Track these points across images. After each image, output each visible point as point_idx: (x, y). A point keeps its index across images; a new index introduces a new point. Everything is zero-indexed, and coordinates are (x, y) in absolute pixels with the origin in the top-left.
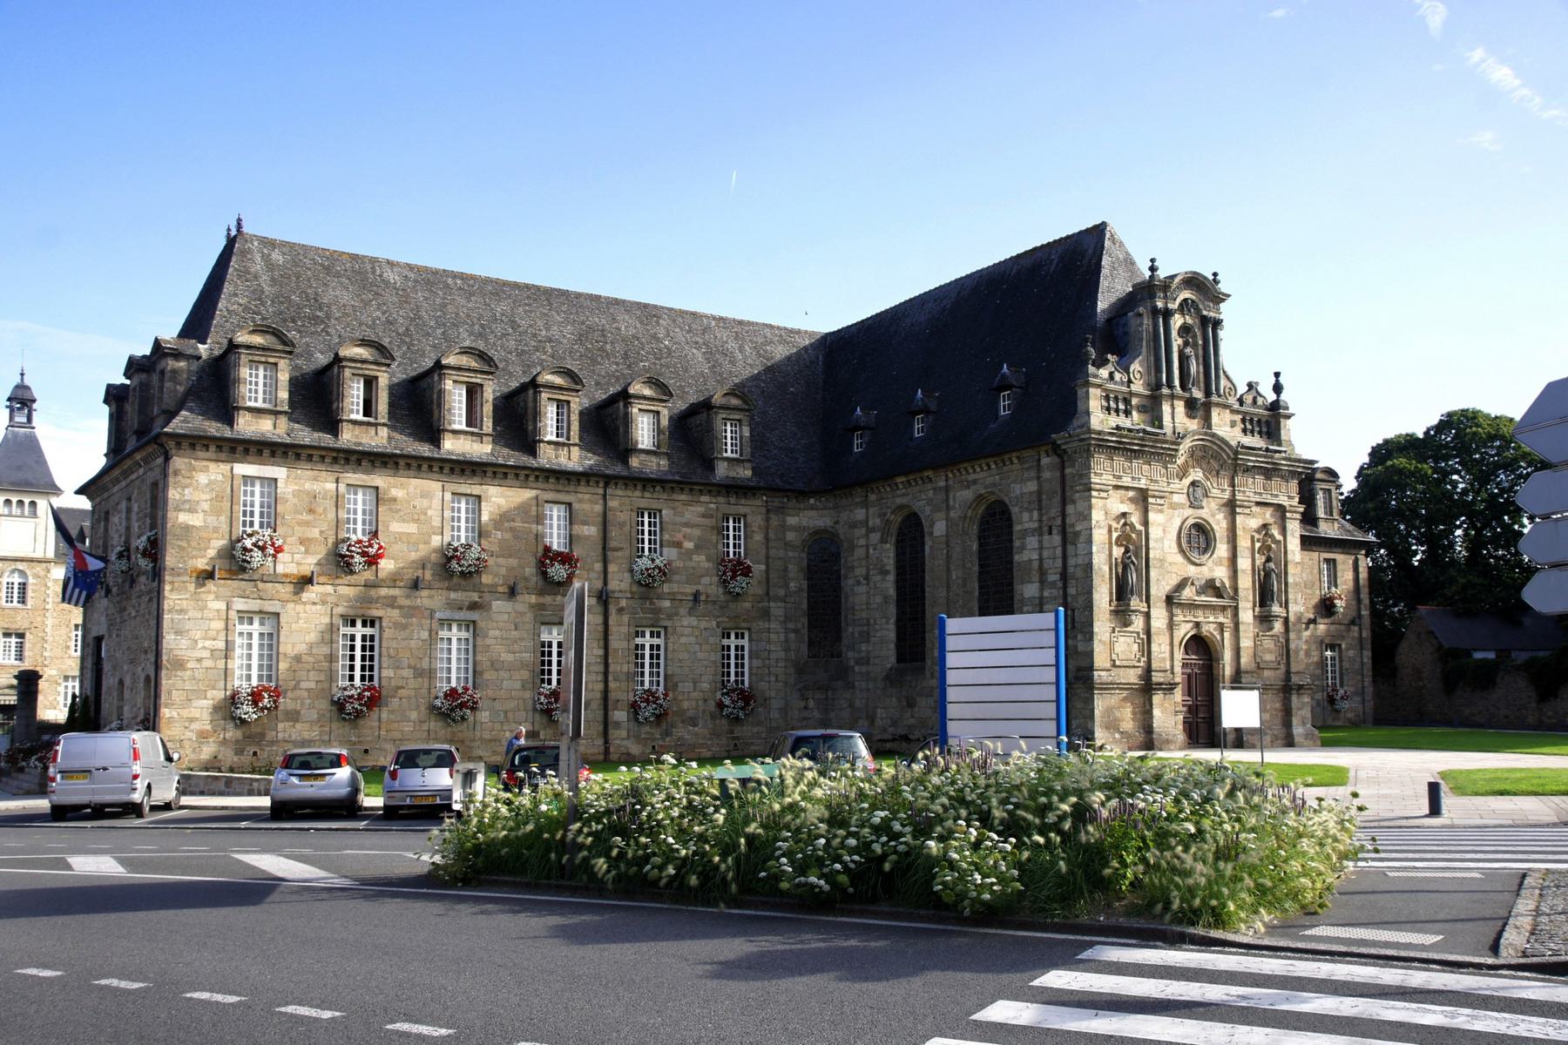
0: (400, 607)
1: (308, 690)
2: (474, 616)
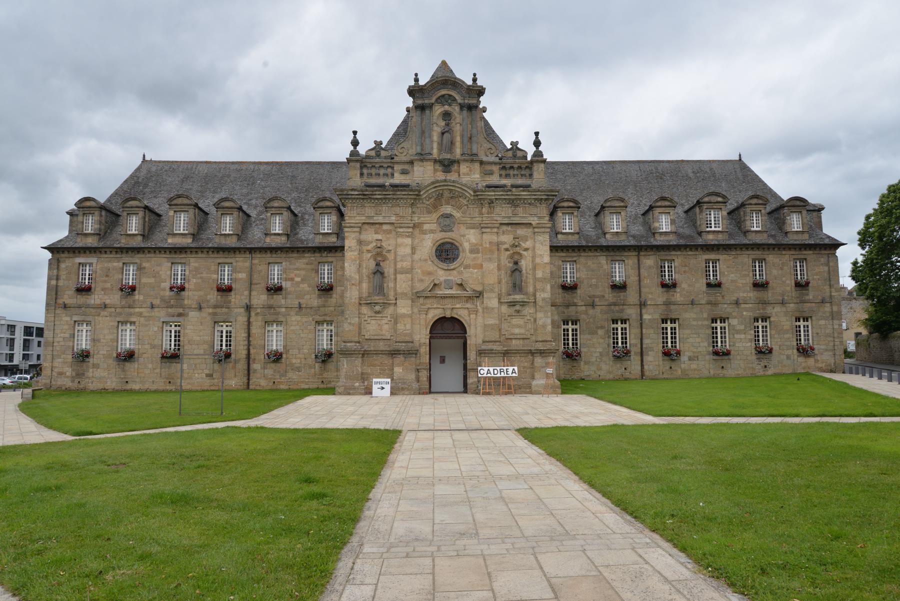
2: (180, 319)
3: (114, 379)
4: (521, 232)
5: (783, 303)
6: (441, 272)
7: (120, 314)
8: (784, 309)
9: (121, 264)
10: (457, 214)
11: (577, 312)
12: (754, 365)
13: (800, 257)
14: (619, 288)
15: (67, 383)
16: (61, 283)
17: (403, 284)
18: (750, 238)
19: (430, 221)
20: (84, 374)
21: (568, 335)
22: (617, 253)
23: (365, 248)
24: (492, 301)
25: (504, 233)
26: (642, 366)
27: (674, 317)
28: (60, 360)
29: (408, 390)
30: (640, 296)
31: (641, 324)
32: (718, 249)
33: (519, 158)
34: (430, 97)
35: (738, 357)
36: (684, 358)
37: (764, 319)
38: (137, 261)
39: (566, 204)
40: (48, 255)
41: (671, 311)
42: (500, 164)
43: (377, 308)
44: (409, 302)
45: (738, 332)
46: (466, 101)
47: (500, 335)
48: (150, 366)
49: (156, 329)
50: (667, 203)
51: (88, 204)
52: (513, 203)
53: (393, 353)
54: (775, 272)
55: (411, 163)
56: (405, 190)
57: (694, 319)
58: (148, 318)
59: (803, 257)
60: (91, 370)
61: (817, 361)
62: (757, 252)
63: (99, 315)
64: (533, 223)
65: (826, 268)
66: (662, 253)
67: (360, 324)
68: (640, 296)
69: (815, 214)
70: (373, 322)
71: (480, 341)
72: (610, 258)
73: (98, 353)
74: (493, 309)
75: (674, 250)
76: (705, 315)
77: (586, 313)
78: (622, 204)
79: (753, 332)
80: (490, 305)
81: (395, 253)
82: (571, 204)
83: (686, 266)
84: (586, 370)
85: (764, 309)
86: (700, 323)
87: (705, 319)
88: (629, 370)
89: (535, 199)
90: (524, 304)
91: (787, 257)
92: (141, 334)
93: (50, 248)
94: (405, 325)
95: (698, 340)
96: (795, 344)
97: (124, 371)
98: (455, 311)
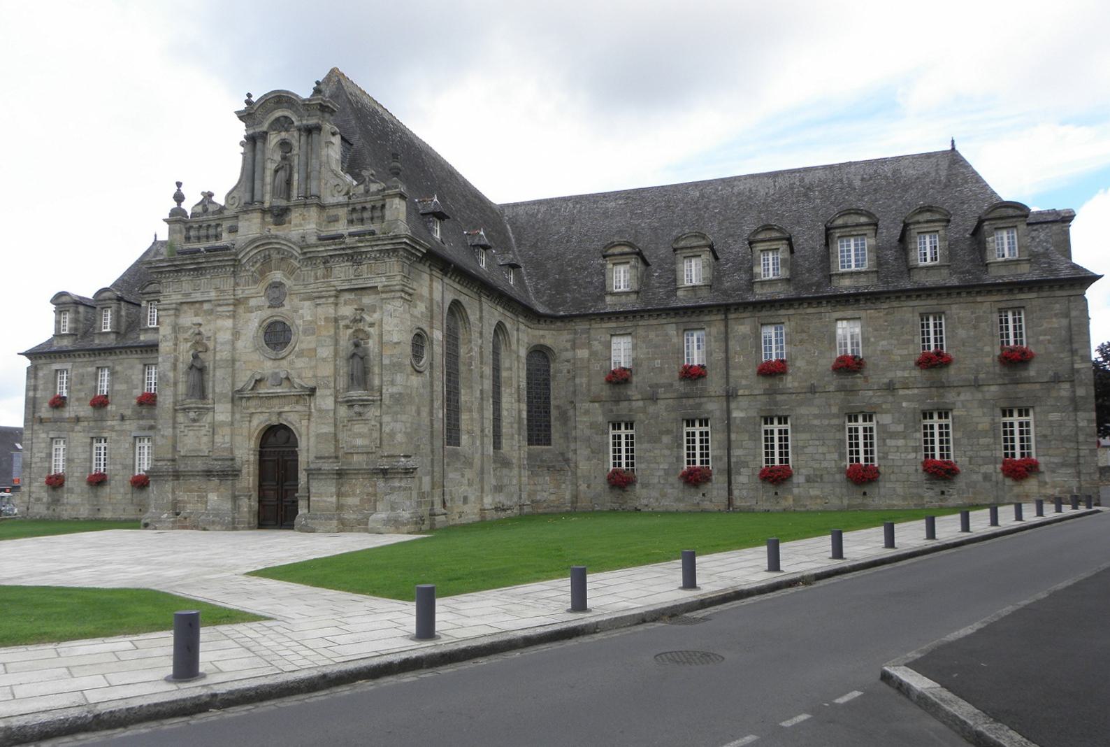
0: (116, 431)
1: (77, 477)
2: (151, 433)
3: (87, 506)
4: (367, 300)
5: (977, 385)
6: (269, 364)
7: (92, 428)
8: (979, 396)
9: (94, 369)
10: (288, 283)
11: (630, 410)
12: (920, 491)
13: (1010, 304)
14: (693, 375)
15: (40, 510)
16: (39, 395)
17: (219, 382)
18: (916, 278)
19: (256, 295)
20: (58, 501)
21: (694, 441)
22: (694, 318)
23: (182, 336)
24: (325, 401)
25: (345, 303)
26: (730, 492)
27: (780, 414)
28: (37, 484)
29: (219, 523)
30: (728, 383)
31: (729, 425)
32: (857, 301)
33: (373, 194)
34: (261, 123)
35: (892, 477)
36: (798, 479)
37: (943, 414)
38: (110, 364)
39: (617, 250)
40: (27, 362)
41: (776, 403)
42: (348, 205)
43: (192, 415)
44: (229, 406)
45: (893, 435)
46: (305, 122)
47: (337, 449)
48: (122, 490)
49: (127, 446)
50: (775, 234)
51: (64, 299)
52: (354, 257)
53: (208, 474)
54: (962, 333)
55: (237, 217)
56: (219, 256)
57: (816, 417)
58: (121, 433)
59: (1016, 304)
60: (65, 496)
61: (1043, 484)
62: (930, 302)
63: (73, 431)
64: (380, 285)
65: (1065, 322)
66: (764, 313)
67: (175, 436)
68: (728, 383)
69: (1055, 227)
70: (191, 433)
71: (312, 458)
72: (682, 327)
73: (72, 476)
74: (327, 411)
75: (782, 306)
76: (835, 410)
77: (644, 410)
78: (703, 242)
79: (920, 435)
80: (324, 407)
81: (215, 339)
82: (627, 249)
83: (803, 331)
84: (642, 495)
85: (942, 396)
86: (826, 422)
87: (834, 416)
88: (708, 496)
89: (380, 251)
90: (365, 403)
91: (986, 306)
92: (113, 452)
93: (30, 354)
94: (224, 436)
95: (824, 449)
96: (1001, 454)
97: (96, 496)
98: (284, 416)
